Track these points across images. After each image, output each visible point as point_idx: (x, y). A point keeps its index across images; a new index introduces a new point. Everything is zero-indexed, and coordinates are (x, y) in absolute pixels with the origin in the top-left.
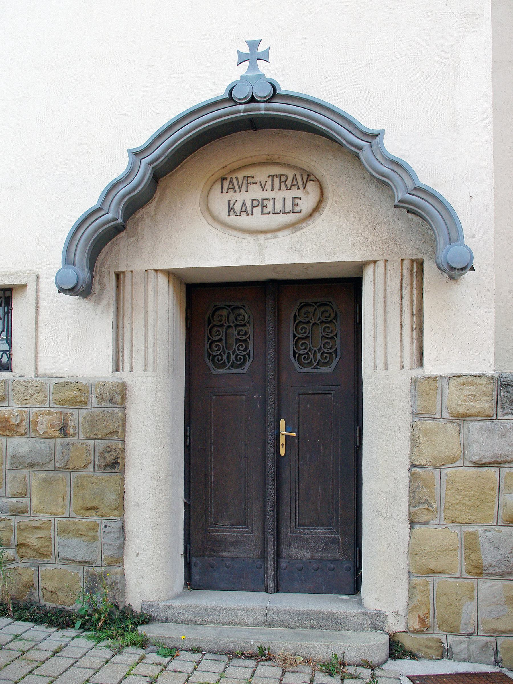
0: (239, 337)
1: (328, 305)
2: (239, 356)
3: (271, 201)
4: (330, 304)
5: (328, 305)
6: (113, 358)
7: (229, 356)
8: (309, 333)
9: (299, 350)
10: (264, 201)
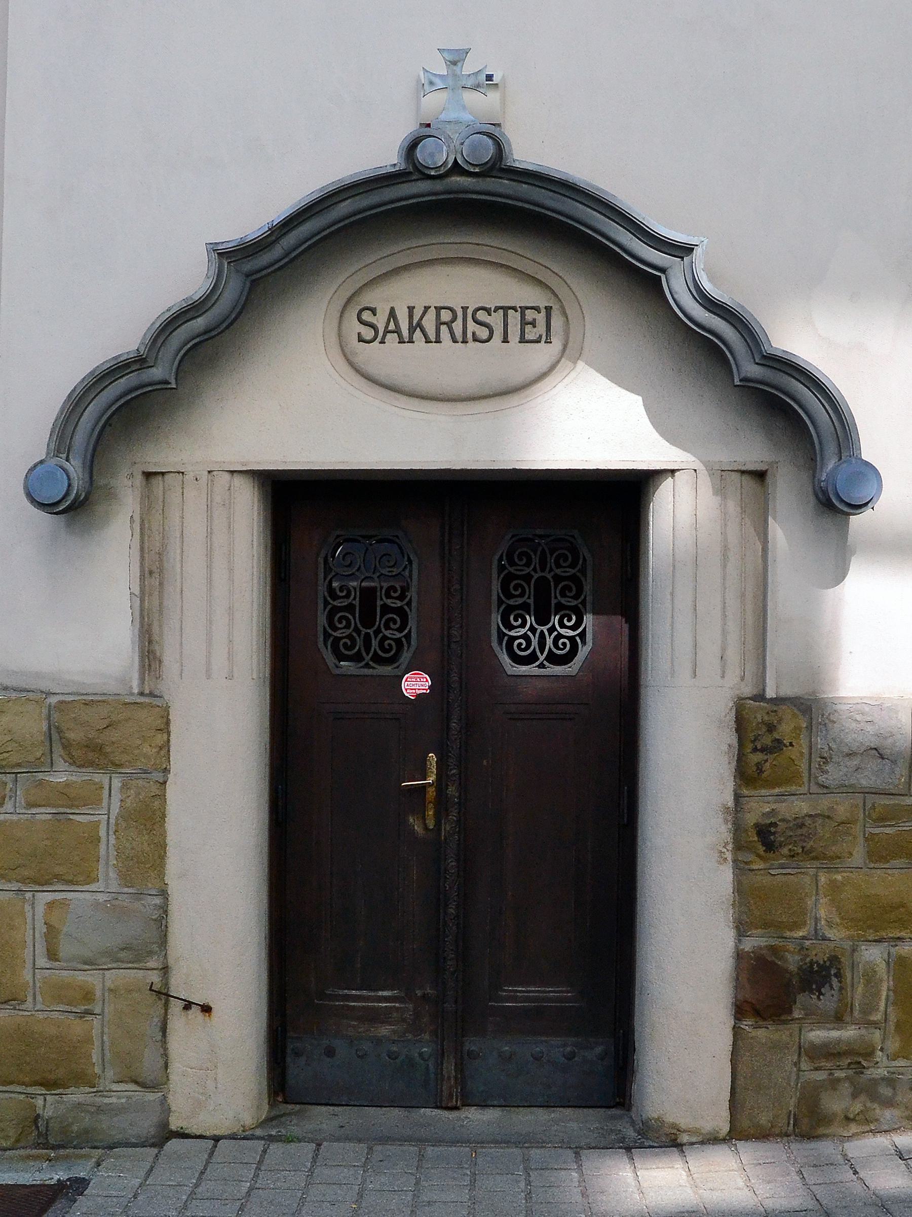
0: (389, 602)
1: (394, 542)
2: (562, 640)
3: (543, 311)
4: (397, 540)
5: (394, 542)
6: (184, 637)
7: (367, 638)
8: (355, 599)
9: (335, 629)
10: (528, 312)
